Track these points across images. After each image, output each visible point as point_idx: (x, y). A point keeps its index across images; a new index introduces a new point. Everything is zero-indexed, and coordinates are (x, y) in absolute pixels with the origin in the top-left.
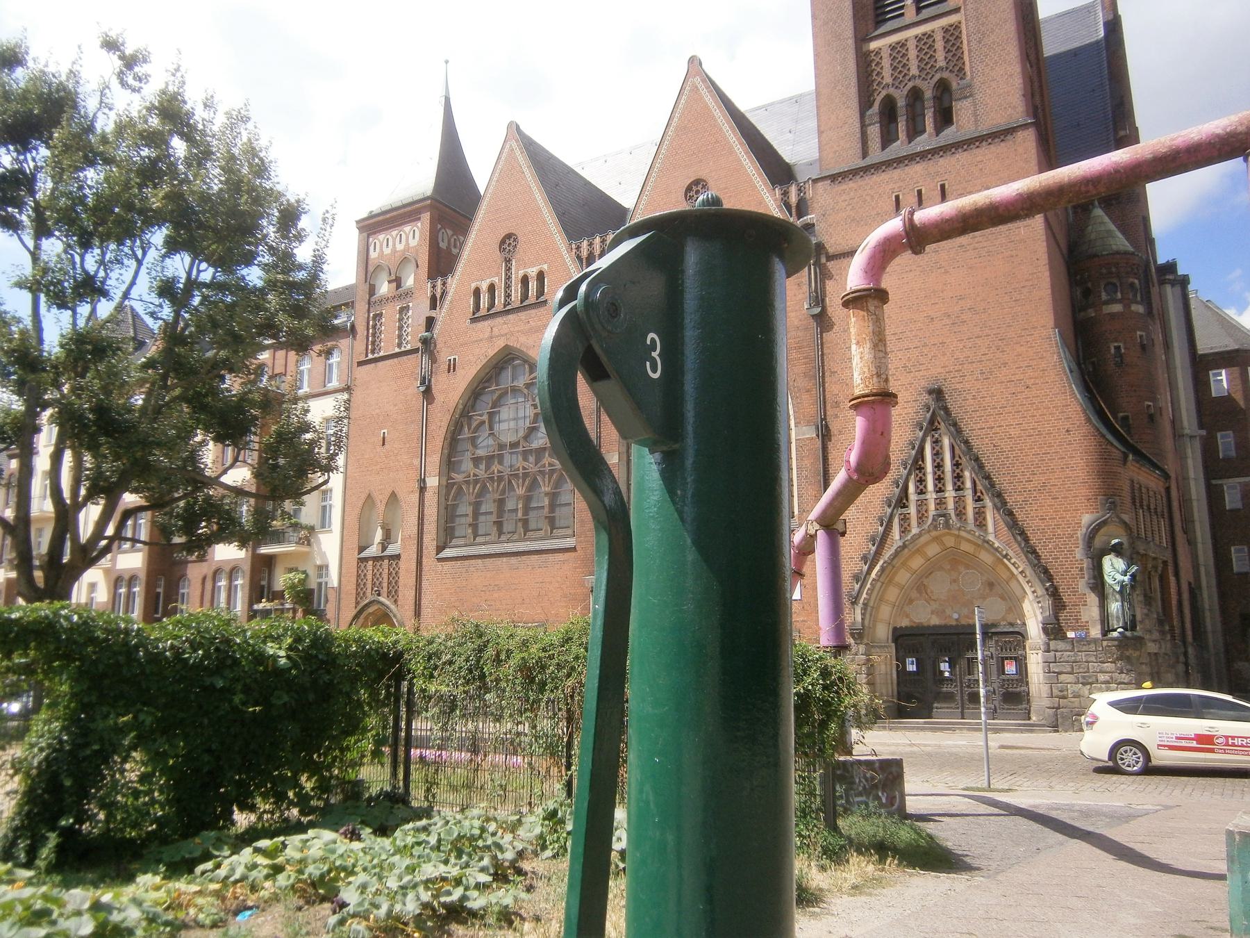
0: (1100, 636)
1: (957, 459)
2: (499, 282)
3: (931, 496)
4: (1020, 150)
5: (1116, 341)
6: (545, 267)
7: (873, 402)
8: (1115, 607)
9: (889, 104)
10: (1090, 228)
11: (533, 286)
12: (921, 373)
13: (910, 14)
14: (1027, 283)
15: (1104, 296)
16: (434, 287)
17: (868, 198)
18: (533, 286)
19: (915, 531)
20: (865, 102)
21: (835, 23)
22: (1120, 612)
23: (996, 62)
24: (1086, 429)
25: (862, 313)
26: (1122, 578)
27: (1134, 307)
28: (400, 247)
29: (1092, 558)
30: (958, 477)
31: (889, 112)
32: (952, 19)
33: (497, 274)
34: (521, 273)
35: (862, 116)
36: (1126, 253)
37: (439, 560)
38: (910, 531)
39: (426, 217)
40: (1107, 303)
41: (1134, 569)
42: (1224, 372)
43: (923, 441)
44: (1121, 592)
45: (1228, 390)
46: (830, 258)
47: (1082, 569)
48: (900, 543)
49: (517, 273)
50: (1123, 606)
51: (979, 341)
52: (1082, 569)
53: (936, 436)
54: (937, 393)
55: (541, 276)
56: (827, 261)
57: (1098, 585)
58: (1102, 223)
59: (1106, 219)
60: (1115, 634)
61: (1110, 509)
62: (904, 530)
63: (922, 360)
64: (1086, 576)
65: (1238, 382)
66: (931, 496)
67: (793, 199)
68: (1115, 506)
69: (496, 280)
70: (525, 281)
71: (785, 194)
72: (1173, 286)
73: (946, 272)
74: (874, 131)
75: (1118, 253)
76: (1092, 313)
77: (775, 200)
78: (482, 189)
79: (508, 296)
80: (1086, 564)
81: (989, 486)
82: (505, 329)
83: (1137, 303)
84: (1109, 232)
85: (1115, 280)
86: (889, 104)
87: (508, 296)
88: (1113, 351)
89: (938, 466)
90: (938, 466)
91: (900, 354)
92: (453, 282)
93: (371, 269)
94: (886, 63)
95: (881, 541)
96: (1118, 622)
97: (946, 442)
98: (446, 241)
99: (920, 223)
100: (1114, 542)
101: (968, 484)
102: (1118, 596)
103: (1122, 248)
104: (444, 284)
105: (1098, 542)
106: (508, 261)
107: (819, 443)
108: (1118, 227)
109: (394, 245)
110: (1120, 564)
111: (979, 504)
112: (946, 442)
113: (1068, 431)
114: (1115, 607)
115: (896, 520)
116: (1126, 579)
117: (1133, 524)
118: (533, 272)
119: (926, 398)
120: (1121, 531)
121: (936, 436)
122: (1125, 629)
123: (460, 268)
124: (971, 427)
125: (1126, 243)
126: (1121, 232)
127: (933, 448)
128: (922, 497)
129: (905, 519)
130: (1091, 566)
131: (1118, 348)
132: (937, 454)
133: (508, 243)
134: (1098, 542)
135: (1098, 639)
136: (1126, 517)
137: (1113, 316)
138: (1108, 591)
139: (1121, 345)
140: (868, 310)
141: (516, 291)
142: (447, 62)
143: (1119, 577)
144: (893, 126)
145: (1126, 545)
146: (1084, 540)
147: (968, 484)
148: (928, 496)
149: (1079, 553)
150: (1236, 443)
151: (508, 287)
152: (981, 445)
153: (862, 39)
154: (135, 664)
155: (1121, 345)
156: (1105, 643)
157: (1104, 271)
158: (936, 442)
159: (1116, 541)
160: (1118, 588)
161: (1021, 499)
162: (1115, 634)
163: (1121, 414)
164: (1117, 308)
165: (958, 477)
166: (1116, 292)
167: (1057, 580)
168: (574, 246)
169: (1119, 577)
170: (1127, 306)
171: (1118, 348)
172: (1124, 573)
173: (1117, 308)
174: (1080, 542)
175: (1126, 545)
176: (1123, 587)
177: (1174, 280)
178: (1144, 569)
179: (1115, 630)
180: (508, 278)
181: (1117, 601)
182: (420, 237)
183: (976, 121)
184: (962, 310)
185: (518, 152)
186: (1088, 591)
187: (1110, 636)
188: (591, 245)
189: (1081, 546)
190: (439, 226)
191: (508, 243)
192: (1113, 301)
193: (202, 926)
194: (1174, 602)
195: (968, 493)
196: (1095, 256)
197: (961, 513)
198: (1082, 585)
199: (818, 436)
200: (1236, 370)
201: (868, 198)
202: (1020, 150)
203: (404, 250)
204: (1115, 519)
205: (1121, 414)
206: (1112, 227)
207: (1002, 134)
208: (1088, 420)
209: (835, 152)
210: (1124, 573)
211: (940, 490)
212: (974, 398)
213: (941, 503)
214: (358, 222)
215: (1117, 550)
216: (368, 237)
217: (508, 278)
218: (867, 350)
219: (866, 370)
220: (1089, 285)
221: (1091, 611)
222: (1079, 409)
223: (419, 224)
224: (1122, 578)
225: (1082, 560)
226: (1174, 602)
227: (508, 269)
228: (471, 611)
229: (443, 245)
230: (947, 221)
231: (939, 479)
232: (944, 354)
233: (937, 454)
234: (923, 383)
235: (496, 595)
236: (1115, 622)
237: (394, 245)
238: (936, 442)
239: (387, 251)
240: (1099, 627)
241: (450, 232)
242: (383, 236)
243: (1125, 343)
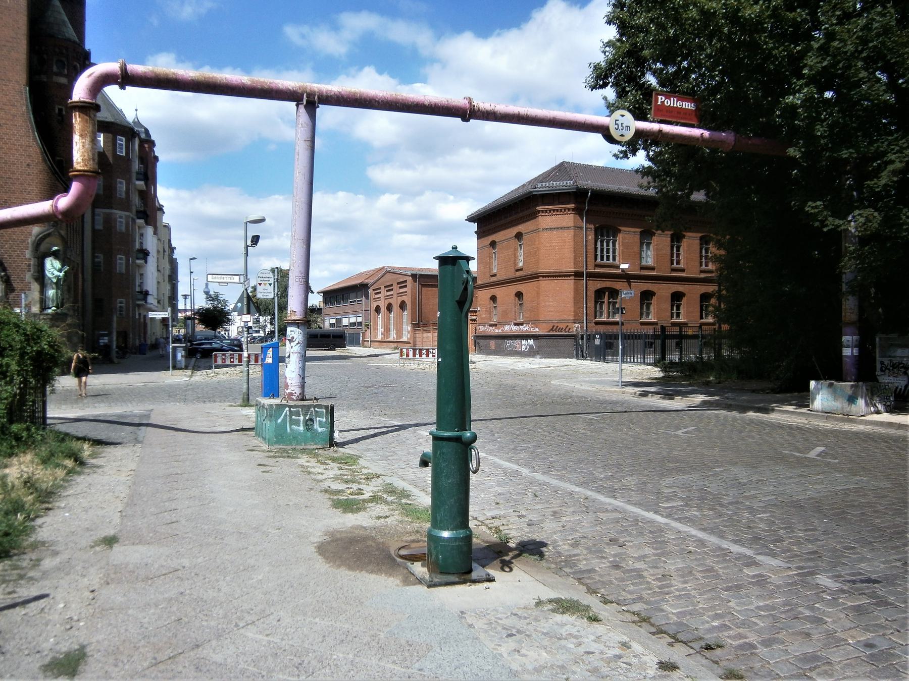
0: (38, 312)
5: (60, 105)
7: (91, 176)
8: (51, 293)
15: (55, 69)
22: (55, 296)
24: (41, 166)
25: (86, 117)
26: (58, 274)
29: (38, 258)
36: (74, 42)
40: (57, 74)
41: (67, 268)
42: (102, 135)
44: (56, 283)
45: (103, 148)
47: (29, 265)
50: (57, 292)
52: (29, 265)
57: (40, 277)
60: (50, 311)
61: (53, 226)
64: (32, 270)
65: (110, 144)
68: (57, 224)
76: (44, 78)
80: (33, 262)
84: (64, 21)
85: (64, 59)
88: (57, 111)
96: (53, 302)
99: (131, 71)
100: (55, 248)
102: (54, 286)
105: (43, 247)
108: (69, 19)
110: (58, 264)
113: (28, 165)
114: (51, 293)
116: (62, 274)
117: (66, 237)
120: (59, 241)
122: (57, 307)
126: (71, 24)
130: (37, 264)
131: (60, 110)
134: (43, 247)
135: (37, 314)
138: (46, 281)
140: (90, 117)
143: (57, 273)
145: (61, 253)
146: (33, 244)
149: (28, 254)
150: (104, 185)
154: (77, 355)
156: (42, 317)
157: (57, 50)
159: (56, 248)
160: (55, 280)
162: (50, 311)
163: (58, 158)
166: (64, 68)
167: (10, 271)
169: (57, 273)
171: (60, 110)
172: (60, 271)
174: (30, 246)
175: (61, 253)
178: (72, 269)
179: (50, 308)
181: (53, 289)
186: (32, 281)
187: (46, 312)
189: (30, 249)
192: (60, 74)
194: (80, 287)
198: (28, 277)
200: (110, 135)
204: (56, 233)
205: (58, 158)
206: (66, 19)
208: (44, 160)
210: (60, 271)
215: (56, 255)
218: (87, 142)
219: (86, 154)
220: (45, 56)
221: (35, 294)
222: (38, 151)
224: (58, 274)
225: (30, 259)
226: (80, 287)
230: (148, 78)
236: (51, 303)
240: (38, 306)
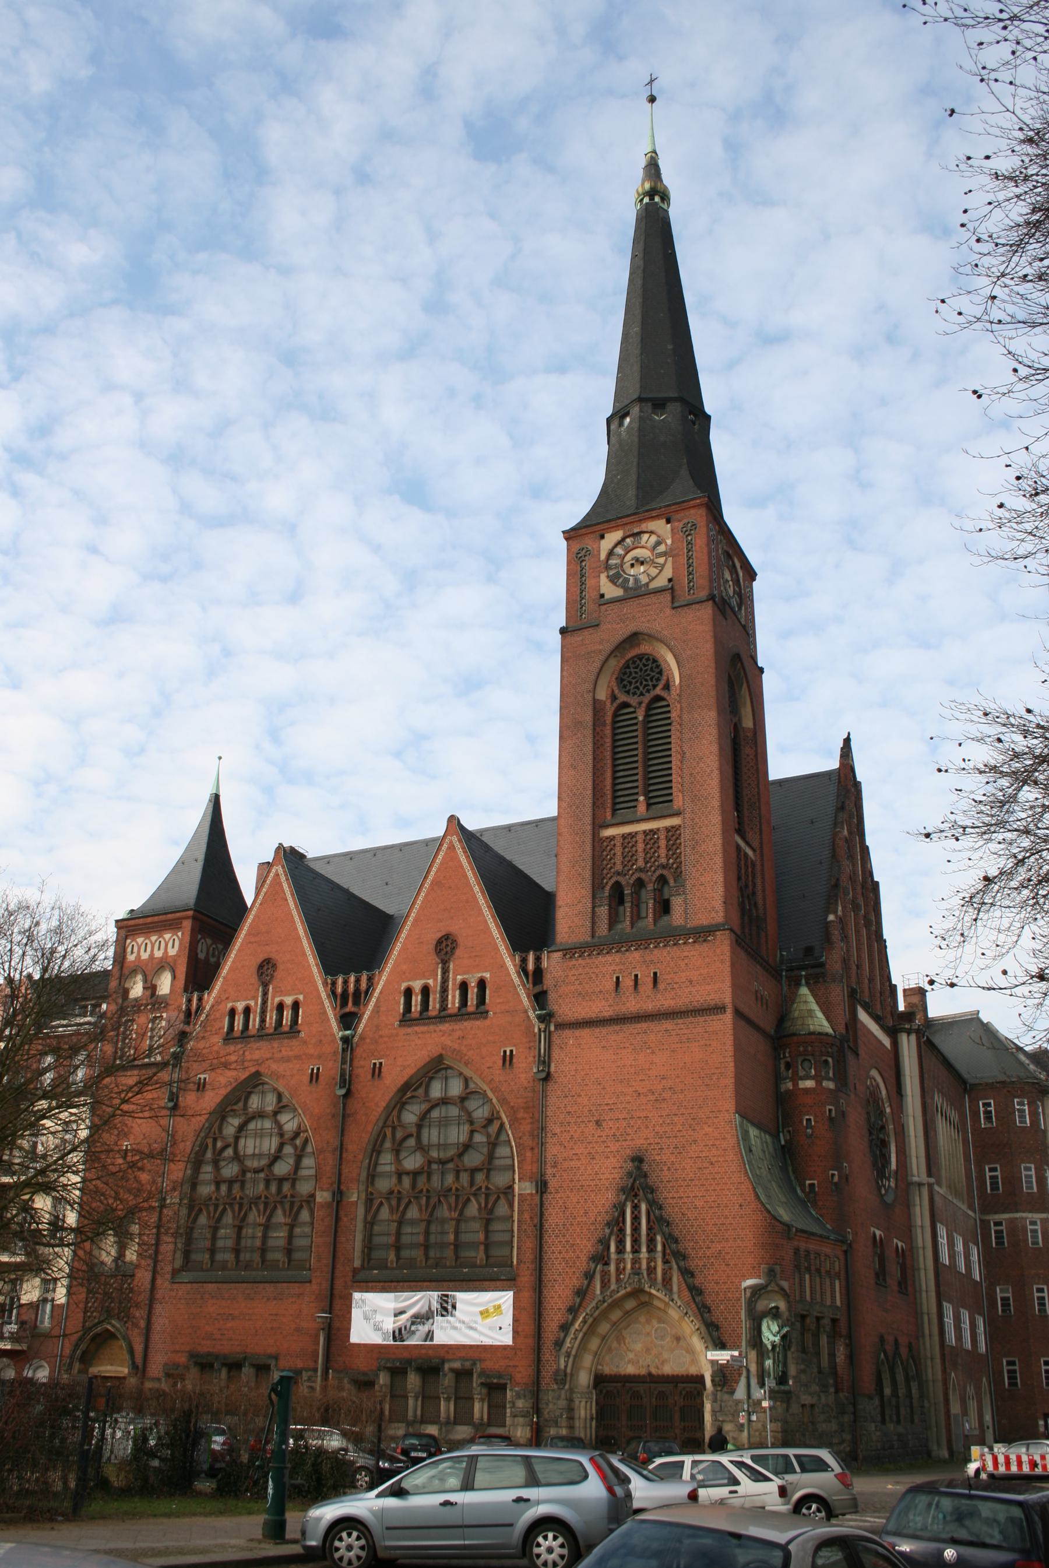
1: (652, 1224)
2: (256, 1004)
3: (629, 1256)
4: (718, 951)
5: (808, 1115)
6: (301, 997)
9: (618, 888)
10: (795, 1005)
11: (287, 1014)
12: (627, 1143)
13: (642, 808)
14: (717, 1071)
16: (189, 1001)
17: (593, 976)
18: (287, 1014)
19: (613, 1287)
20: (596, 886)
21: (577, 807)
23: (705, 870)
27: (825, 1084)
28: (158, 954)
30: (651, 1241)
31: (618, 896)
32: (675, 821)
33: (255, 998)
34: (277, 1000)
35: (594, 897)
36: (827, 1034)
37: (674, 608)
38: (609, 1287)
39: (187, 924)
41: (786, 1329)
43: (624, 1205)
46: (560, 1026)
48: (600, 1298)
49: (273, 999)
51: (676, 1119)
53: (636, 1201)
54: (638, 1160)
55: (296, 1005)
56: (556, 1028)
58: (806, 1002)
59: (811, 999)
62: (605, 1285)
63: (628, 1130)
66: (629, 1256)
67: (531, 966)
69: (252, 1003)
70: (280, 1007)
71: (524, 961)
72: (909, 1034)
73: (653, 1053)
74: (603, 911)
75: (813, 1033)
77: (515, 966)
78: (249, 904)
79: (263, 1021)
81: (675, 1254)
82: (257, 1055)
83: (829, 1079)
85: (810, 1058)
86: (618, 888)
87: (263, 1021)
89: (636, 1229)
90: (636, 1229)
91: (611, 1124)
92: (210, 998)
93: (126, 971)
94: (618, 850)
95: (582, 1293)
97: (643, 1207)
98: (205, 950)
101: (659, 1248)
103: (818, 1029)
104: (200, 999)
105: (762, 1305)
106: (265, 986)
107: (537, 1198)
109: (152, 950)
111: (667, 1266)
112: (643, 1207)
114: (769, 1363)
115: (598, 1277)
118: (289, 1000)
119: (630, 1165)
121: (636, 1201)
123: (218, 985)
124: (667, 1196)
125: (825, 1023)
127: (632, 1213)
128: (621, 1256)
129: (605, 1274)
131: (809, 1120)
132: (636, 1219)
133: (266, 969)
136: (785, 1284)
137: (806, 1090)
139: (812, 1118)
141: (271, 1018)
142: (220, 758)
143: (772, 1338)
144: (621, 908)
147: (659, 1248)
148: (626, 1256)
151: (263, 1012)
152: (671, 1211)
153: (598, 825)
155: (812, 1118)
158: (636, 1207)
161: (701, 1263)
164: (809, 1084)
165: (651, 1241)
166: (811, 1068)
168: (329, 981)
169: (772, 1338)
170: (819, 1083)
173: (809, 1084)
176: (774, 1346)
177: (910, 1029)
180: (264, 1002)
182: (180, 944)
183: (686, 918)
184: (664, 1089)
185: (283, 878)
188: (346, 982)
190: (199, 936)
191: (266, 969)
192: (808, 1077)
193: (581, 593)
195: (659, 1256)
196: (794, 1034)
197: (651, 1270)
199: (537, 1192)
201: (593, 976)
202: (718, 951)
203: (162, 958)
206: (815, 1007)
207: (702, 934)
209: (570, 927)
211: (636, 1250)
212: (669, 1169)
213: (636, 1261)
214: (117, 921)
216: (126, 938)
217: (264, 1002)
223: (180, 934)
227: (265, 994)
228: (203, 1339)
229: (202, 956)
231: (636, 1241)
232: (647, 1127)
233: (636, 1219)
234: (628, 1152)
235: (229, 1325)
237: (152, 950)
238: (636, 1207)
239: (145, 956)
241: (209, 941)
242: (142, 939)
243: (816, 1116)
